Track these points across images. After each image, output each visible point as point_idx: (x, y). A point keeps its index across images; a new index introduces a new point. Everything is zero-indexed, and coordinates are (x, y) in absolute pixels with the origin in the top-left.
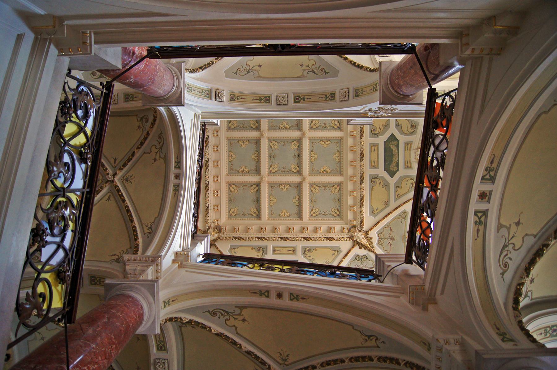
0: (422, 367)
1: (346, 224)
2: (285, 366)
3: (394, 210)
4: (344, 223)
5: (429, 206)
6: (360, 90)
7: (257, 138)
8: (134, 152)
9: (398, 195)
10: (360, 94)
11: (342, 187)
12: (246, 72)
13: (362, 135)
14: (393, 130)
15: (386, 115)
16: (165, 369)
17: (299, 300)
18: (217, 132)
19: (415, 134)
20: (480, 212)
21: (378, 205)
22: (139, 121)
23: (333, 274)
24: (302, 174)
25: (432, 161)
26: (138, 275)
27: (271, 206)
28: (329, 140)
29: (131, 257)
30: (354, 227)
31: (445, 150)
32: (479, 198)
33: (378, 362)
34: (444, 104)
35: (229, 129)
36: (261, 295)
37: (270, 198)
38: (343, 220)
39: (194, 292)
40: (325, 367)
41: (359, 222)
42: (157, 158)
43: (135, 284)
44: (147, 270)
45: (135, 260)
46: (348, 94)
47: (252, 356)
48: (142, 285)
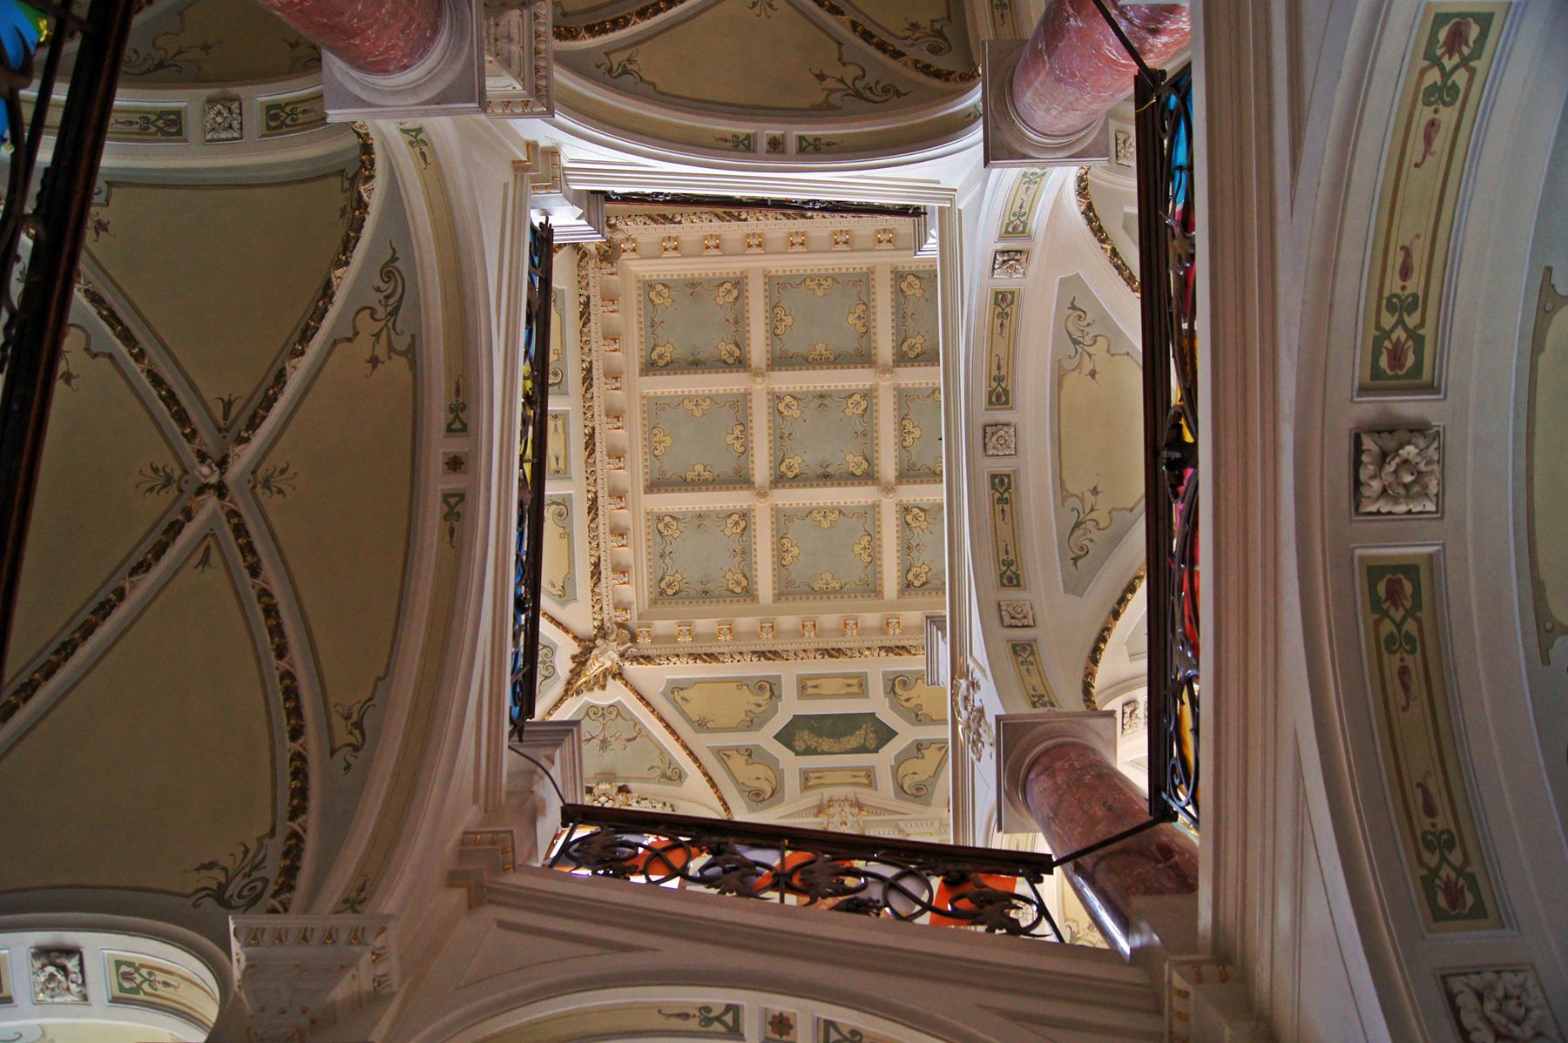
0: (292, 882)
1: (640, 617)
2: (251, 485)
3: (685, 747)
4: (641, 610)
5: (733, 869)
6: (1031, 658)
7: (874, 358)
8: (842, 13)
9: (728, 756)
10: (1020, 659)
11: (742, 599)
12: (1076, 334)
13: (888, 650)
14: (907, 734)
15: (960, 727)
16: (213, 129)
17: (446, 520)
18: (889, 241)
19: (897, 796)
20: (736, 1019)
21: (697, 703)
22: (932, 26)
23: (520, 605)
24: (776, 487)
25: (857, 873)
26: (496, 46)
27: (683, 401)
28: (874, 560)
29: (545, 24)
30: (634, 638)
31: (892, 909)
32: (774, 1017)
33: (289, 756)
34: (1015, 902)
35: (899, 276)
36: (451, 410)
37: (705, 397)
38: (650, 606)
39: (451, 214)
40: (259, 601)
41: (646, 653)
42: (830, 83)
43: (472, 42)
44: (511, 74)
45: (538, 35)
46: (1020, 624)
47: (273, 387)
48: (469, 64)
